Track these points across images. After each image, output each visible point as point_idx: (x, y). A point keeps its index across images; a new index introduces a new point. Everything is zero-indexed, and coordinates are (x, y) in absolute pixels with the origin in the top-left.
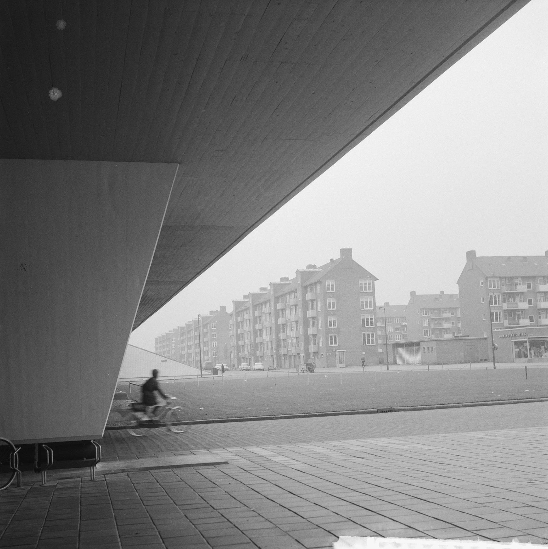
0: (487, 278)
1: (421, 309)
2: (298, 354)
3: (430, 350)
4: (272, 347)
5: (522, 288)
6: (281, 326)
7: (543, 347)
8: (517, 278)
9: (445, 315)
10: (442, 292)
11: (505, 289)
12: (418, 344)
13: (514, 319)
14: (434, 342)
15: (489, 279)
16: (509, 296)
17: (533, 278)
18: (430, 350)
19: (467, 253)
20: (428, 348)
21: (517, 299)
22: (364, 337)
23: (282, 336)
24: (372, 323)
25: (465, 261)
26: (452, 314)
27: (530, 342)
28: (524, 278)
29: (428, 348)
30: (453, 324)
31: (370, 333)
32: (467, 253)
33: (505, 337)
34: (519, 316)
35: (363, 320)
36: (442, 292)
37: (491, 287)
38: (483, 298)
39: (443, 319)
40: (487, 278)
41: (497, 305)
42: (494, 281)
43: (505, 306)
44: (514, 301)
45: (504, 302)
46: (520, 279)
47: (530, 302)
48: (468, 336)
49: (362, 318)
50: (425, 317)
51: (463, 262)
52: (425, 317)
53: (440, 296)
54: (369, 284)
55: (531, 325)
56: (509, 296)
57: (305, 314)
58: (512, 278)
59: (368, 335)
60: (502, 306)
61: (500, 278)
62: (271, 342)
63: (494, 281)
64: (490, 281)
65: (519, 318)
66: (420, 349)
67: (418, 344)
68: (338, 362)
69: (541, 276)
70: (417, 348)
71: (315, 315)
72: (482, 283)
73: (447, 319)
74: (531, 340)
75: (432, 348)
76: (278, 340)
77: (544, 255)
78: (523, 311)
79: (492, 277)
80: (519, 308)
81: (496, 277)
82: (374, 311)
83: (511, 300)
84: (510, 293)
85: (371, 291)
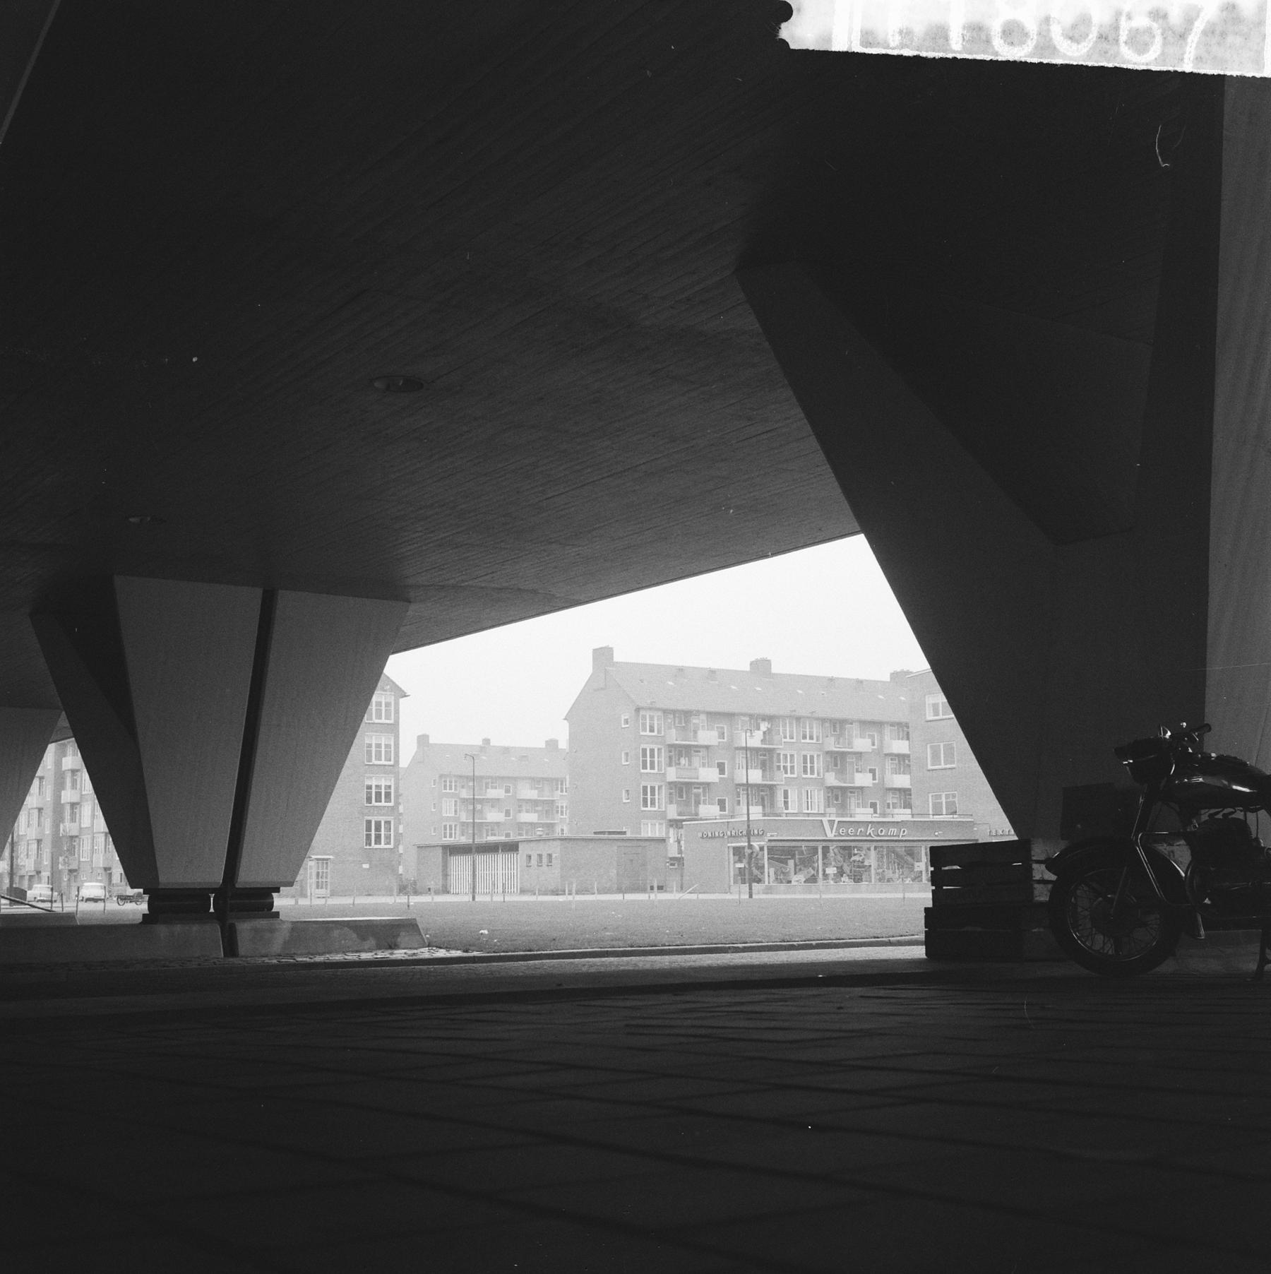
0: (638, 710)
1: (441, 776)
2: (38, 872)
3: (545, 860)
4: (39, 855)
5: (707, 736)
6: (68, 808)
7: (791, 863)
8: (698, 713)
9: (492, 793)
10: (487, 741)
11: (673, 737)
12: (512, 847)
13: (687, 803)
14: (558, 843)
15: (642, 713)
16: (680, 752)
17: (730, 716)
18: (545, 860)
19: (595, 651)
20: (540, 856)
21: (696, 761)
22: (369, 829)
23: (68, 827)
24: (388, 795)
25: (591, 671)
26: (507, 791)
27: (770, 850)
28: (713, 716)
29: (540, 856)
30: (508, 813)
31: (383, 819)
32: (595, 651)
33: (713, 837)
34: (697, 796)
35: (369, 787)
36: (487, 741)
37: (645, 730)
38: (627, 754)
39: (488, 800)
40: (638, 710)
41: (656, 771)
42: (652, 718)
43: (672, 774)
44: (690, 761)
45: (670, 765)
46: (703, 717)
47: (721, 768)
48: (624, 833)
49: (368, 782)
50: (447, 795)
51: (585, 669)
52: (447, 795)
53: (482, 749)
54: (388, 705)
55: (722, 817)
56: (680, 752)
57: (57, 797)
58: (687, 714)
59: (378, 825)
60: (664, 774)
61: (665, 711)
62: (39, 841)
63: (652, 718)
64: (644, 717)
65: (698, 803)
66: (519, 858)
67: (512, 847)
68: (314, 886)
69: (744, 715)
70: (508, 855)
71: (75, 800)
72: (626, 722)
73: (495, 802)
74: (773, 844)
75: (550, 856)
76: (57, 840)
77: (748, 669)
78: (707, 786)
79: (650, 709)
80: (701, 780)
81: (658, 709)
82: (393, 769)
83: (683, 761)
84: (680, 746)
85: (392, 721)
